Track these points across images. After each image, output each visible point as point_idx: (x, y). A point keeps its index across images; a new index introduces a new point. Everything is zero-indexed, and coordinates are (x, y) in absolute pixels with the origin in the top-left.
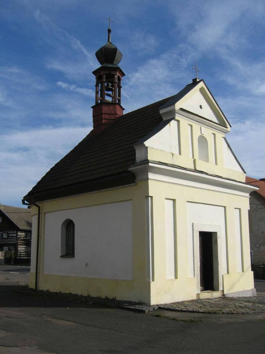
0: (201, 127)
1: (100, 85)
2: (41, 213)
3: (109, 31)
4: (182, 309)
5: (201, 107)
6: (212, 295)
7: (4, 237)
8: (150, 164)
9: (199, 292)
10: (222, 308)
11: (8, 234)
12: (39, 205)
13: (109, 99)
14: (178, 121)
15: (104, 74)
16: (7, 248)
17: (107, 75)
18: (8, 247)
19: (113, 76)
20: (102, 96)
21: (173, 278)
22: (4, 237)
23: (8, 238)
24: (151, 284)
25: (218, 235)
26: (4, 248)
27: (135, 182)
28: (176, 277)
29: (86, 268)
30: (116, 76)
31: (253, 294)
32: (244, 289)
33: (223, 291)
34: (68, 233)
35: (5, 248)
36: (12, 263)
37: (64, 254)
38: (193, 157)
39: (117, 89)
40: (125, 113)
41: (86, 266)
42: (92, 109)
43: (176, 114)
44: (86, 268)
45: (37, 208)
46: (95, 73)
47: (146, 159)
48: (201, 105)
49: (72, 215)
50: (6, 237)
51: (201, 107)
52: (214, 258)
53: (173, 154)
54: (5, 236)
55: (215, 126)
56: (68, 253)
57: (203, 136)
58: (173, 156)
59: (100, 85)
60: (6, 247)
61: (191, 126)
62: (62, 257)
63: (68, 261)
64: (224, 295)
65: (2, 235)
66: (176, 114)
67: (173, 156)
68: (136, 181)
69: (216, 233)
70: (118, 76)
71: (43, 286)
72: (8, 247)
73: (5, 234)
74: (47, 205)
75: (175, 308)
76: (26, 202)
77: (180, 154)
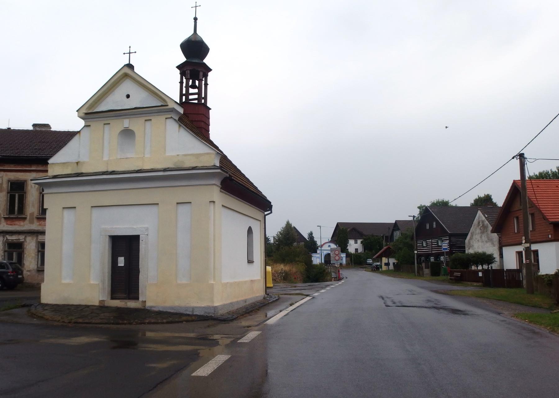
16: (443, 258)
35: (442, 258)
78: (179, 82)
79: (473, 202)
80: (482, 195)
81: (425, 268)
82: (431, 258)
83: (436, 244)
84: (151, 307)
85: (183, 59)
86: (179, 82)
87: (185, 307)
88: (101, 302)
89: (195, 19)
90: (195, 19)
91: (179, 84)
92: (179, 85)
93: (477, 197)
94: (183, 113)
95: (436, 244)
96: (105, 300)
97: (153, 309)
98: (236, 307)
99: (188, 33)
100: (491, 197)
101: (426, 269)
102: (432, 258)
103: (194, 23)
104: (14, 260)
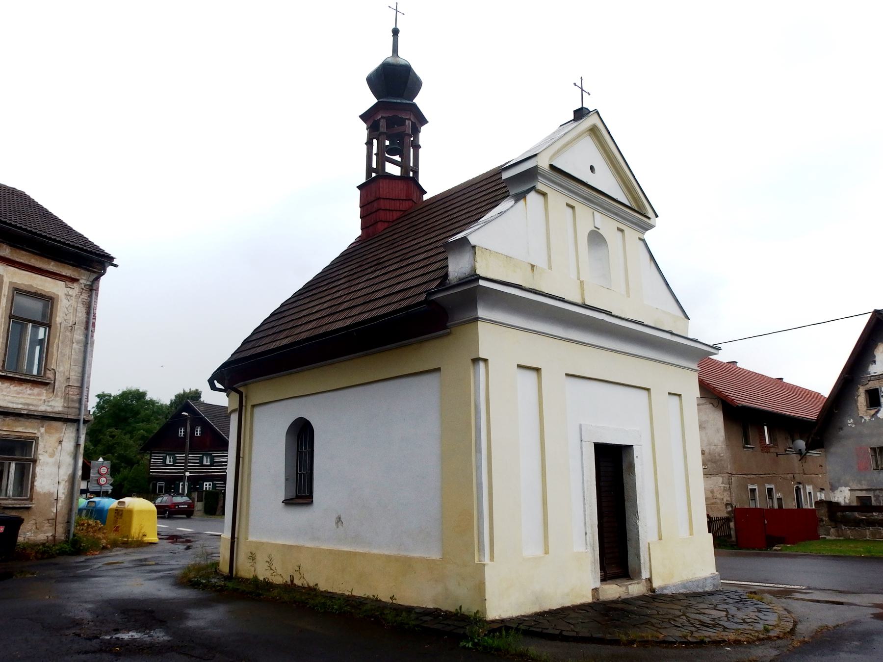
0: (593, 213)
1: (375, 141)
2: (246, 406)
3: (390, 7)
4: (564, 633)
5: (592, 168)
6: (627, 588)
7: (205, 463)
8: (482, 283)
9: (597, 584)
10: (659, 626)
11: (212, 458)
12: (241, 389)
13: (393, 170)
14: (544, 194)
15: (382, 117)
16: (210, 485)
17: (387, 119)
18: (211, 483)
19: (402, 122)
20: (382, 161)
21: (540, 552)
22: (205, 463)
23: (211, 465)
24: (488, 571)
25: (636, 451)
26: (205, 483)
27: (446, 328)
28: (546, 552)
29: (338, 527)
30: (409, 124)
31: (714, 585)
32: (127, 388)
33: (650, 580)
34: (301, 448)
35: (206, 485)
36: (217, 513)
37: (292, 494)
38: (579, 279)
39: (412, 150)
40: (426, 197)
41: (337, 523)
42: (359, 192)
43: (539, 178)
44: (338, 527)
45: (237, 395)
46: (364, 117)
47: (473, 273)
48: (593, 165)
49: (306, 409)
50: (208, 464)
51: (592, 168)
52: (627, 504)
53: (533, 266)
54: (206, 461)
55: (625, 212)
56: (300, 492)
57: (598, 232)
58: (533, 270)
59: (375, 141)
60: (208, 483)
61: (573, 207)
62: (288, 502)
63: (300, 516)
64: (653, 590)
65: (201, 459)
66: (539, 178)
67: (533, 270)
68: (448, 324)
69: (630, 447)
70: (412, 122)
71: (244, 569)
72: (211, 483)
73: (207, 459)
74: (257, 392)
75: (547, 629)
76: (218, 386)
77: (550, 268)
78: (366, 144)
79: (173, 398)
80: (141, 391)
81: (198, 501)
82: (205, 483)
83: (189, 464)
84: (663, 588)
85: (371, 100)
86: (366, 144)
87: (372, 600)
88: (655, 589)
89: (396, 32)
90: (396, 32)
91: (366, 146)
92: (364, 148)
93: (182, 392)
94: (424, 200)
95: (189, 464)
96: (598, 588)
97: (666, 592)
98: (155, 597)
99: (380, 55)
100: (201, 394)
101: (199, 503)
102: (206, 485)
103: (392, 38)
104: (870, 495)
